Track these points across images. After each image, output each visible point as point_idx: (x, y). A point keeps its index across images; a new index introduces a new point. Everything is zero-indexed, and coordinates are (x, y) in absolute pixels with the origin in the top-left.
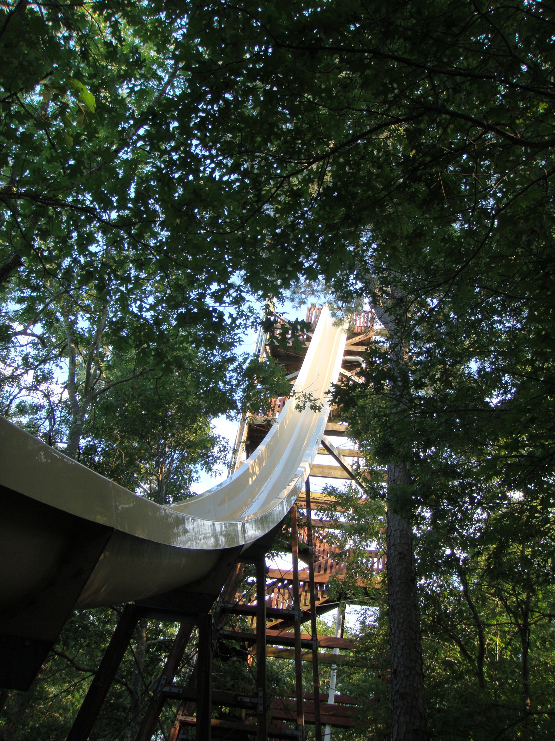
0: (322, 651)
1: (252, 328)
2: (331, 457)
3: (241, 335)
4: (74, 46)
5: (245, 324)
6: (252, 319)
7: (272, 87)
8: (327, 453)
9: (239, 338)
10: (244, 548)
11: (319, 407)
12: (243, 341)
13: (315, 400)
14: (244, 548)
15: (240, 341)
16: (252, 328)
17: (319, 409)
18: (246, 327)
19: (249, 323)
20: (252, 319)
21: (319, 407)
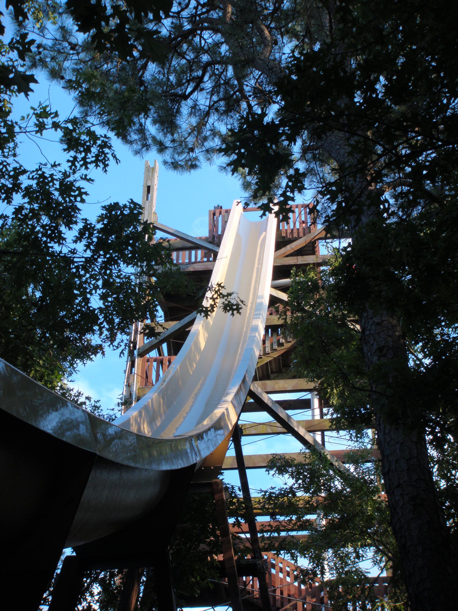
0: (262, 519)
1: (97, 166)
2: (290, 438)
3: (81, 184)
4: (368, 604)
5: (84, 159)
6: (94, 150)
7: (357, 5)
8: (284, 430)
9: (79, 189)
10: (197, 468)
11: (237, 305)
12: (86, 193)
13: (229, 295)
14: (197, 468)
15: (81, 194)
16: (97, 166)
17: (238, 309)
18: (86, 164)
19: (91, 157)
20: (94, 150)
21: (237, 305)
